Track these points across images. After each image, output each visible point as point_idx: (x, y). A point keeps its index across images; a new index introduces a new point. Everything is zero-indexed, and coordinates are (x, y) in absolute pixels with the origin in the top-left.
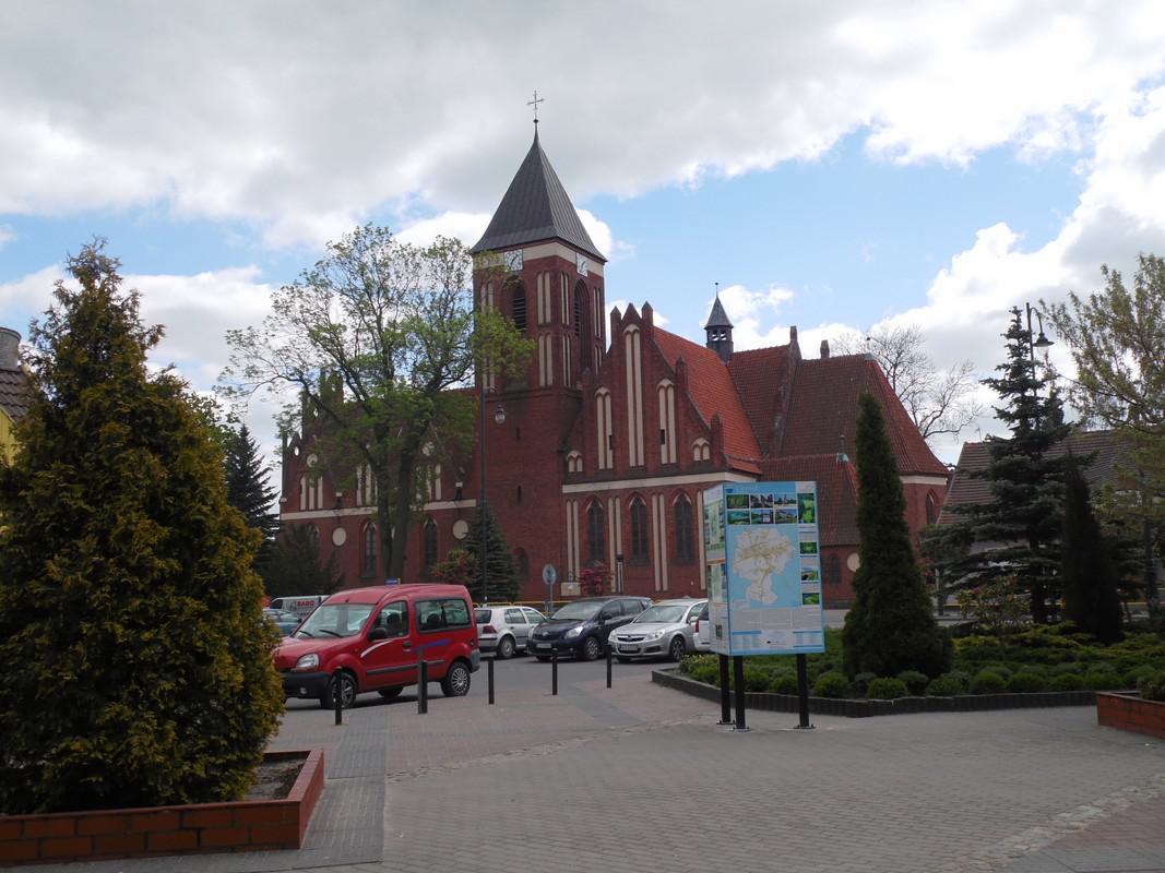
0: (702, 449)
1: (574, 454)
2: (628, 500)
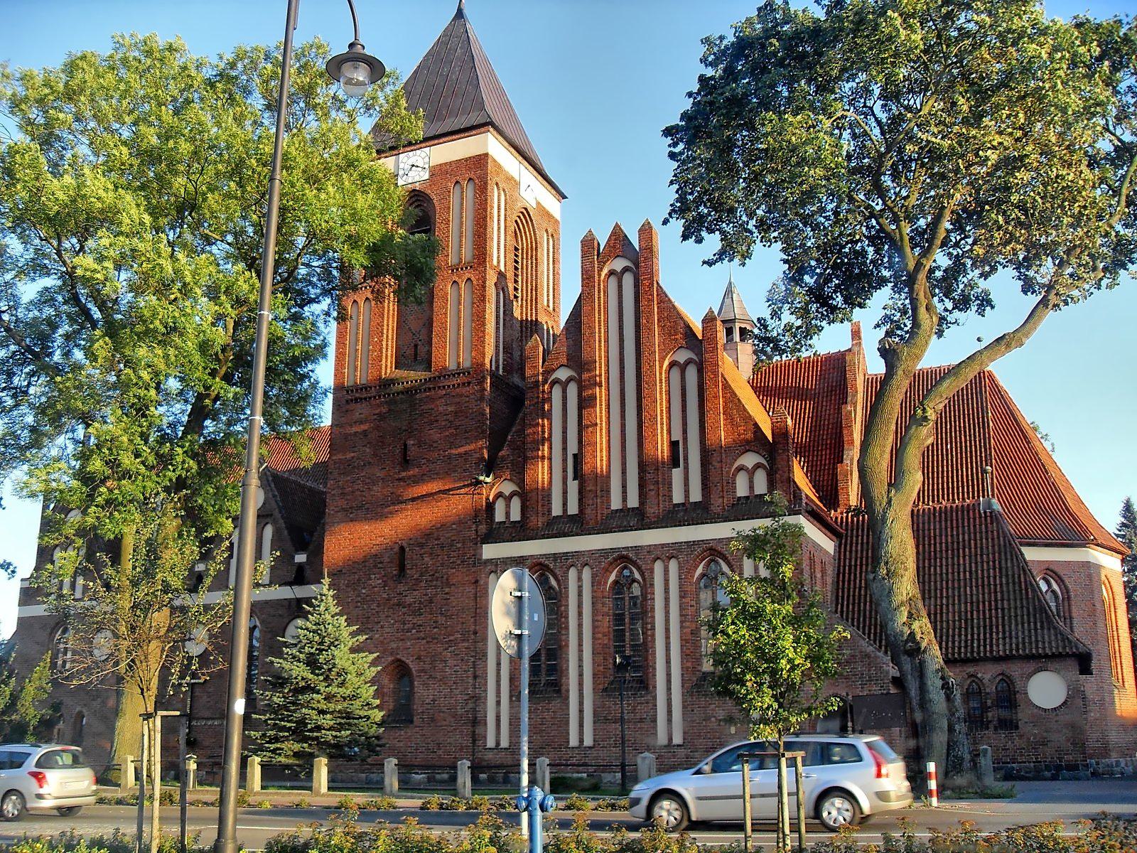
0: (751, 473)
2: (607, 571)
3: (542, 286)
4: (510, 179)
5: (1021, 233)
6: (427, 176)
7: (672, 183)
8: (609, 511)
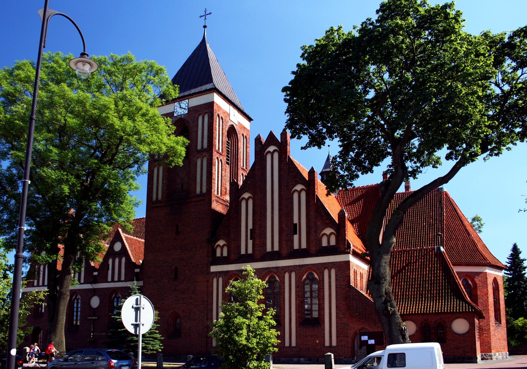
0: (222, 248)
1: (221, 243)
3: (240, 158)
4: (225, 112)
5: (513, 135)
6: (187, 112)
7: (286, 113)
8: (265, 252)
